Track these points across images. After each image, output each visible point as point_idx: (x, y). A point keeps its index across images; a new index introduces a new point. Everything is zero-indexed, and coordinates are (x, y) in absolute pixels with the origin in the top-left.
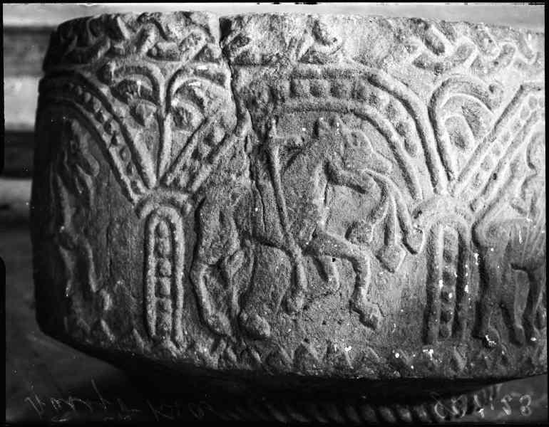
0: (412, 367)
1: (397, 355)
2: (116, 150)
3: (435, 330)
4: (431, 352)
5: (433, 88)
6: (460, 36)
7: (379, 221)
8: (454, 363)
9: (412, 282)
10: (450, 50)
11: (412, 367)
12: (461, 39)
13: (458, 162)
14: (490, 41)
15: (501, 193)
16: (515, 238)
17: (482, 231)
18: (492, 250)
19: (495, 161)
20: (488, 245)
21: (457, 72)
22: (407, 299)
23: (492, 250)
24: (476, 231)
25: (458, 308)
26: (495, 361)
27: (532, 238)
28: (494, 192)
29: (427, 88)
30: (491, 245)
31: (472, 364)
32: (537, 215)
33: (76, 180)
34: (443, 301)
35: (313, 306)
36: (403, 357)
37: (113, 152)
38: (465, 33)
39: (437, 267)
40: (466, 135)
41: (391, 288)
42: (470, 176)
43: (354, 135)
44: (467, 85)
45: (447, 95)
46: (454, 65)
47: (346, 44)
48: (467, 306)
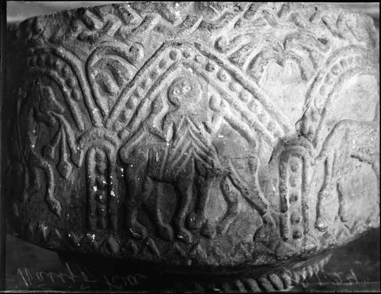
0: (79, 245)
1: (69, 235)
2: (226, 84)
3: (93, 221)
4: (94, 236)
5: (89, 53)
6: (106, 15)
7: (56, 145)
8: (109, 246)
9: (77, 186)
10: (98, 25)
11: (79, 245)
12: (107, 16)
13: (109, 103)
14: (129, 15)
15: (141, 125)
16: (153, 158)
17: (126, 154)
18: (132, 166)
19: (135, 102)
20: (128, 162)
21: (105, 40)
22: (74, 198)
23: (132, 166)
24: (120, 152)
25: (108, 208)
26: (142, 249)
27: (170, 159)
28: (137, 122)
29: (84, 54)
30: (131, 163)
31: (123, 249)
32: (176, 141)
33: (82, 125)
34: (97, 202)
35: (311, 274)
36: (73, 237)
37: (73, 102)
38: (110, 12)
39: (90, 176)
40: (108, 84)
41: (65, 190)
42: (117, 113)
43: (44, 89)
44: (109, 48)
45: (96, 59)
46: (100, 36)
47: (45, 32)
48: (115, 208)
